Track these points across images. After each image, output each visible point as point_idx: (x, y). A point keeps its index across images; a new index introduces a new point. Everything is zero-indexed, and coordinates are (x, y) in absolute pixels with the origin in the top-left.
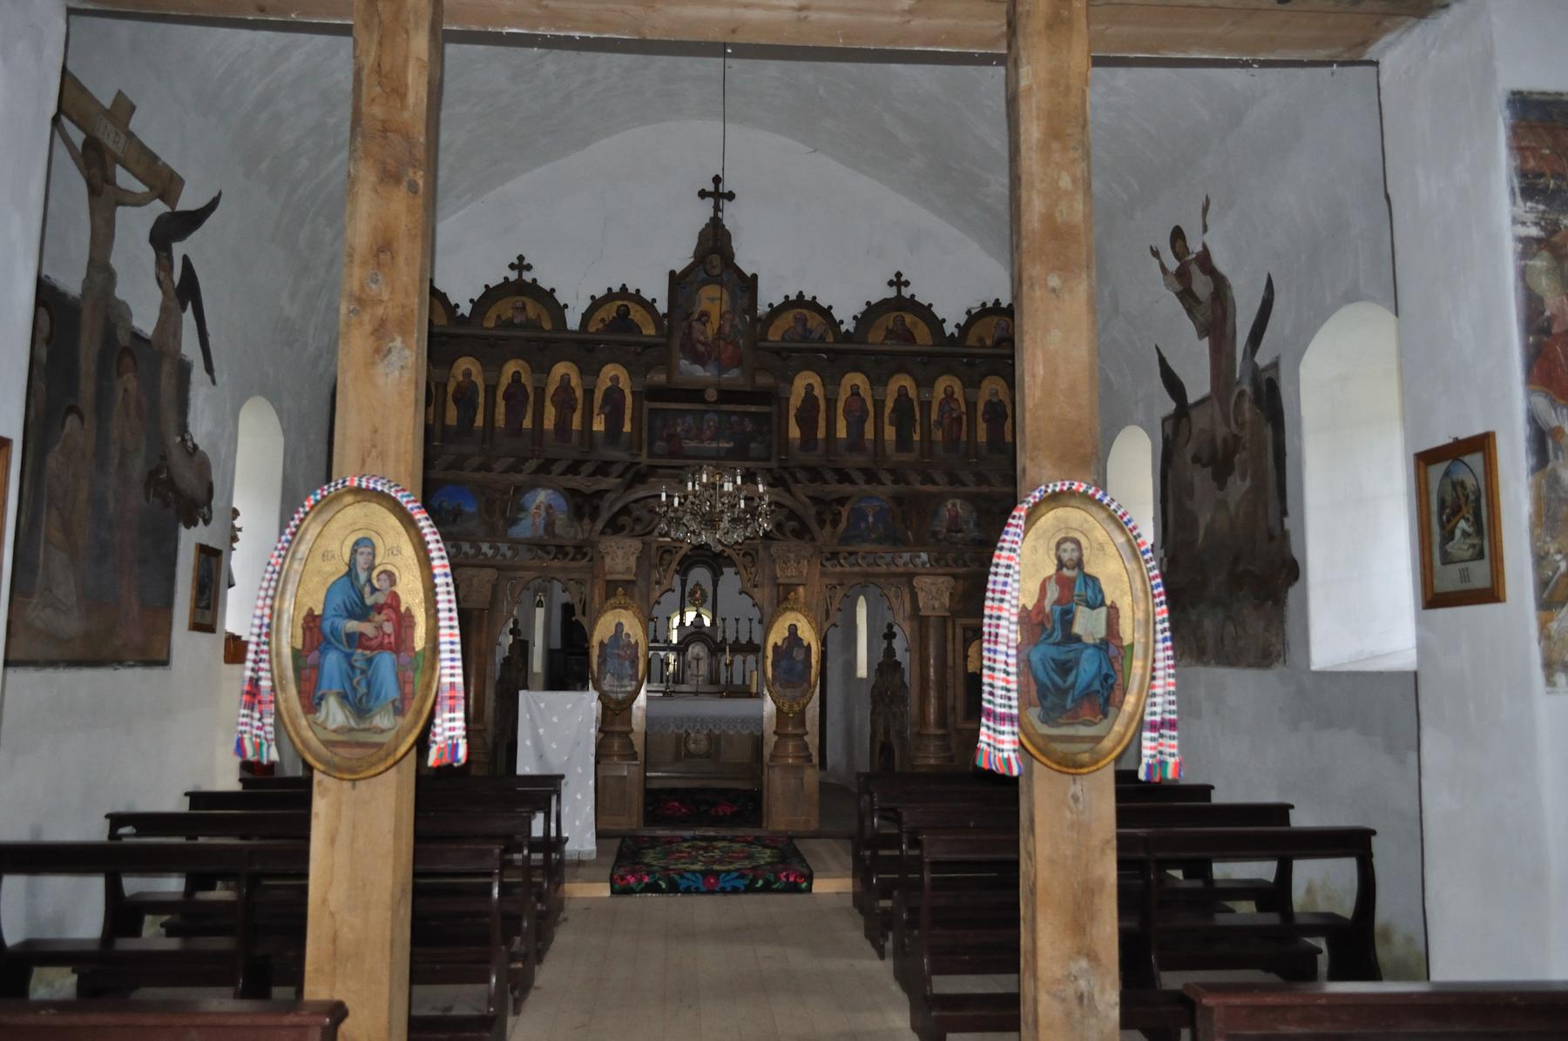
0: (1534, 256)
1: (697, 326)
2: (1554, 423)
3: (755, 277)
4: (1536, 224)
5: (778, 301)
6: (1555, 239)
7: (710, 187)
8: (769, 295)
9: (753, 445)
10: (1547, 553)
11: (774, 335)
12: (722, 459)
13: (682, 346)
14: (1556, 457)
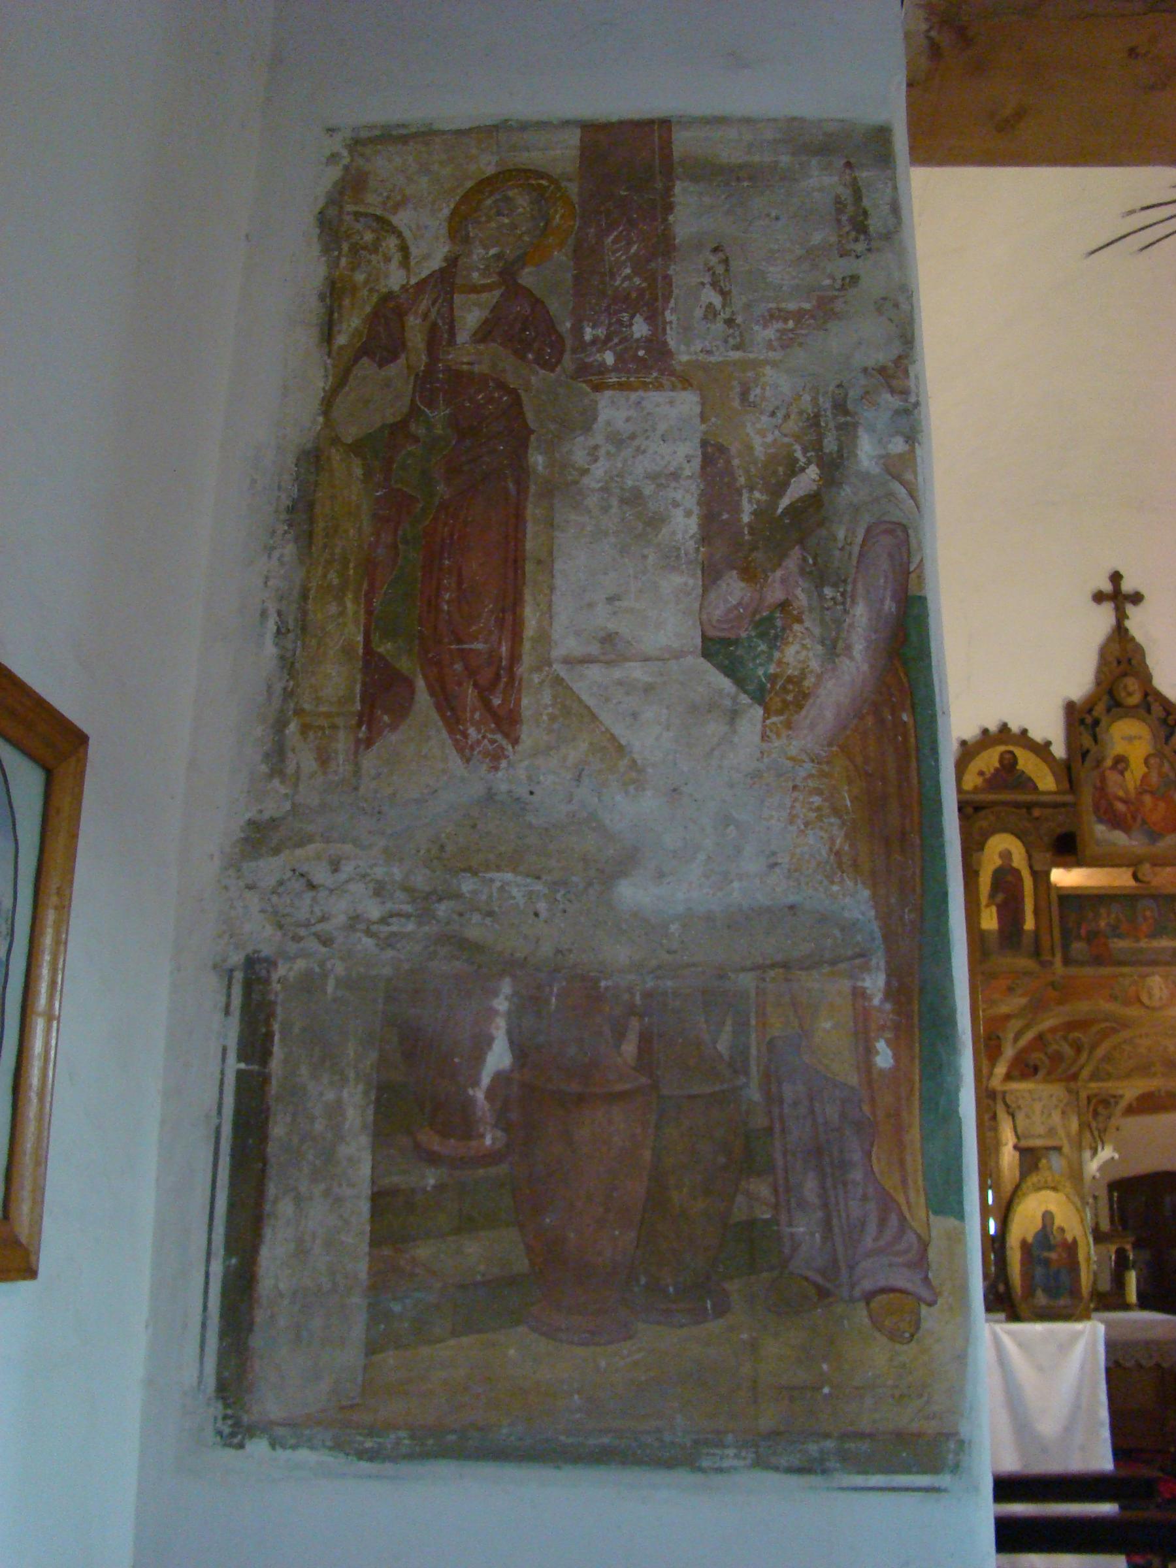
1: (1113, 777)
7: (1107, 587)
13: (1097, 808)
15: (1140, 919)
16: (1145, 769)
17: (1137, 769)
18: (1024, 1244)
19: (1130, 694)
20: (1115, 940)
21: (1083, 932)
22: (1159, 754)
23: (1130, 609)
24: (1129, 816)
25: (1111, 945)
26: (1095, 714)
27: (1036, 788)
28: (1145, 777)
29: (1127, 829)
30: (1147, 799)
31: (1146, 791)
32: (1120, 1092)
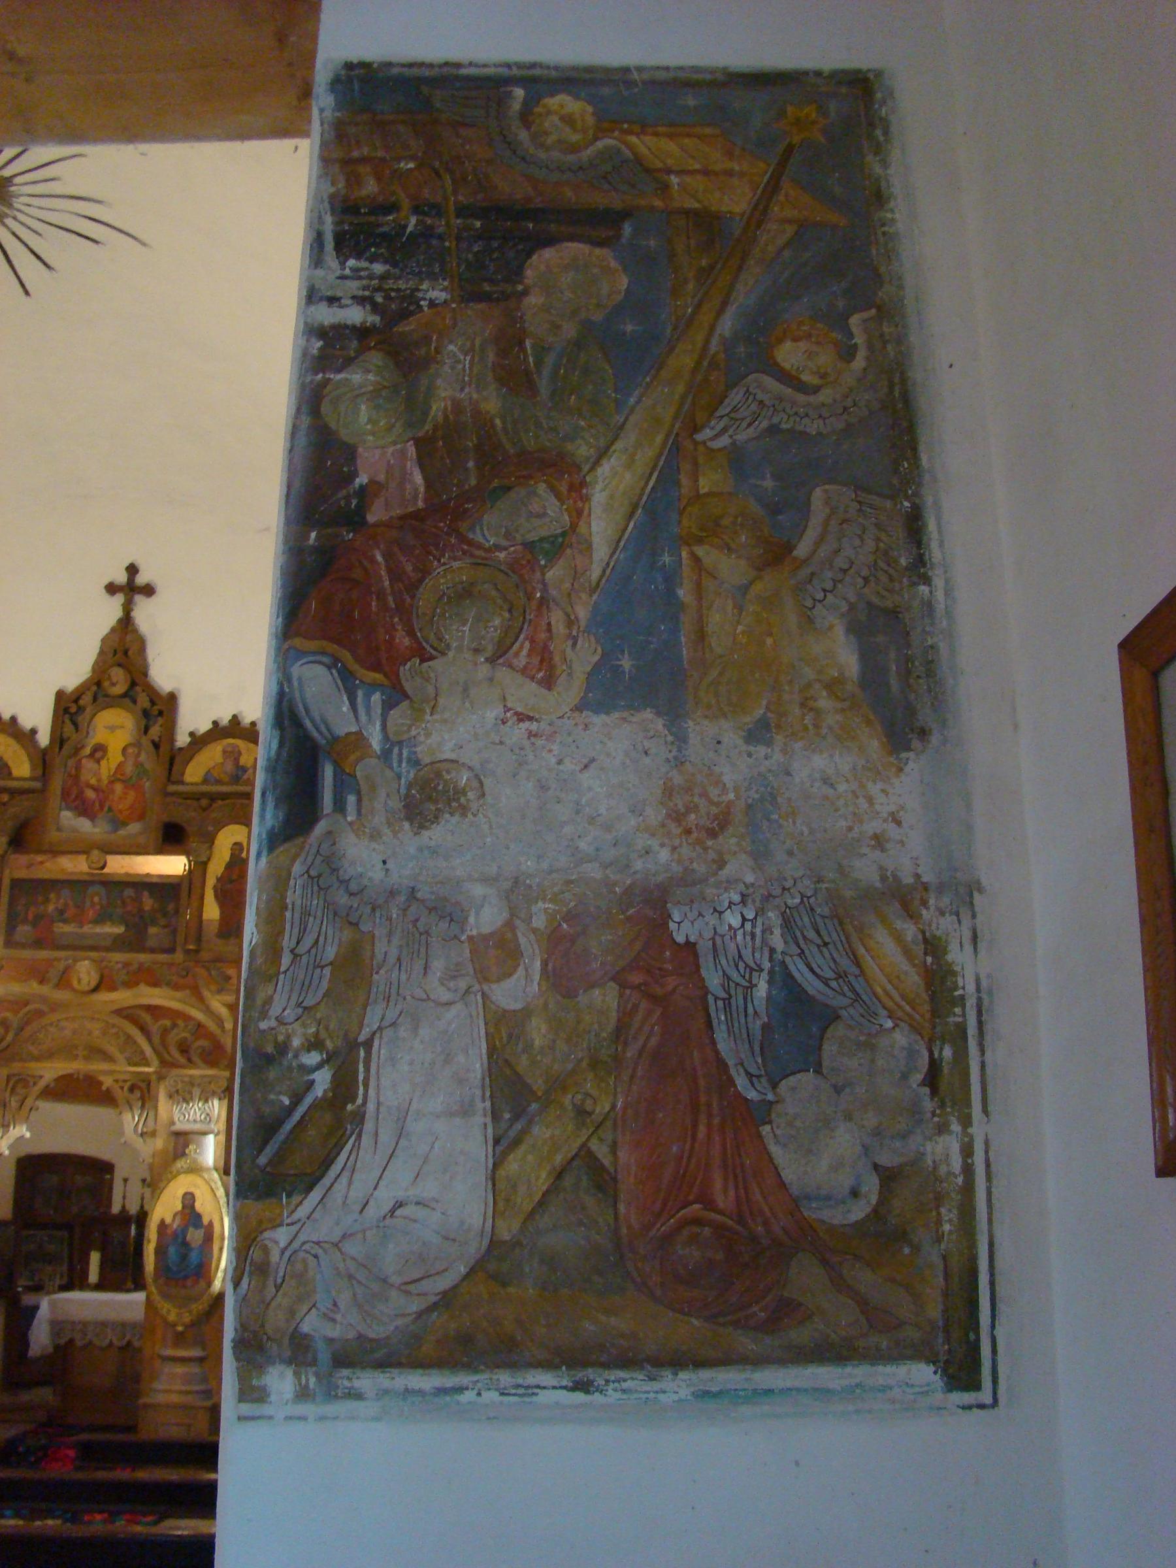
0: (348, 362)
1: (88, 764)
2: (344, 726)
3: (172, 698)
4: (360, 300)
5: (204, 727)
6: (407, 327)
7: (141, 580)
8: (193, 719)
9: (152, 930)
10: (283, 1048)
11: (194, 773)
12: (108, 949)
13: (65, 794)
14: (340, 806)
15: (88, 904)
16: (122, 759)
17: (114, 757)
18: (162, 1225)
19: (114, 684)
20: (61, 925)
21: (30, 917)
22: (137, 744)
23: (139, 599)
24: (97, 804)
25: (55, 929)
26: (81, 702)
27: (10, 773)
28: (120, 765)
29: (92, 817)
30: (119, 788)
31: (119, 780)
32: (41, 1073)
